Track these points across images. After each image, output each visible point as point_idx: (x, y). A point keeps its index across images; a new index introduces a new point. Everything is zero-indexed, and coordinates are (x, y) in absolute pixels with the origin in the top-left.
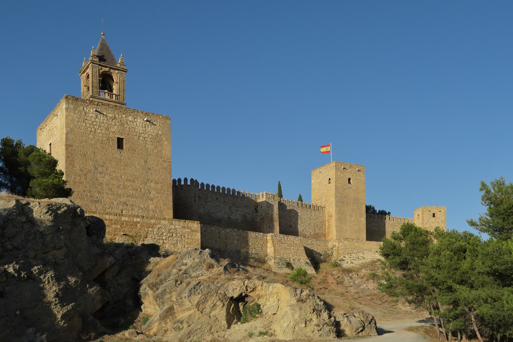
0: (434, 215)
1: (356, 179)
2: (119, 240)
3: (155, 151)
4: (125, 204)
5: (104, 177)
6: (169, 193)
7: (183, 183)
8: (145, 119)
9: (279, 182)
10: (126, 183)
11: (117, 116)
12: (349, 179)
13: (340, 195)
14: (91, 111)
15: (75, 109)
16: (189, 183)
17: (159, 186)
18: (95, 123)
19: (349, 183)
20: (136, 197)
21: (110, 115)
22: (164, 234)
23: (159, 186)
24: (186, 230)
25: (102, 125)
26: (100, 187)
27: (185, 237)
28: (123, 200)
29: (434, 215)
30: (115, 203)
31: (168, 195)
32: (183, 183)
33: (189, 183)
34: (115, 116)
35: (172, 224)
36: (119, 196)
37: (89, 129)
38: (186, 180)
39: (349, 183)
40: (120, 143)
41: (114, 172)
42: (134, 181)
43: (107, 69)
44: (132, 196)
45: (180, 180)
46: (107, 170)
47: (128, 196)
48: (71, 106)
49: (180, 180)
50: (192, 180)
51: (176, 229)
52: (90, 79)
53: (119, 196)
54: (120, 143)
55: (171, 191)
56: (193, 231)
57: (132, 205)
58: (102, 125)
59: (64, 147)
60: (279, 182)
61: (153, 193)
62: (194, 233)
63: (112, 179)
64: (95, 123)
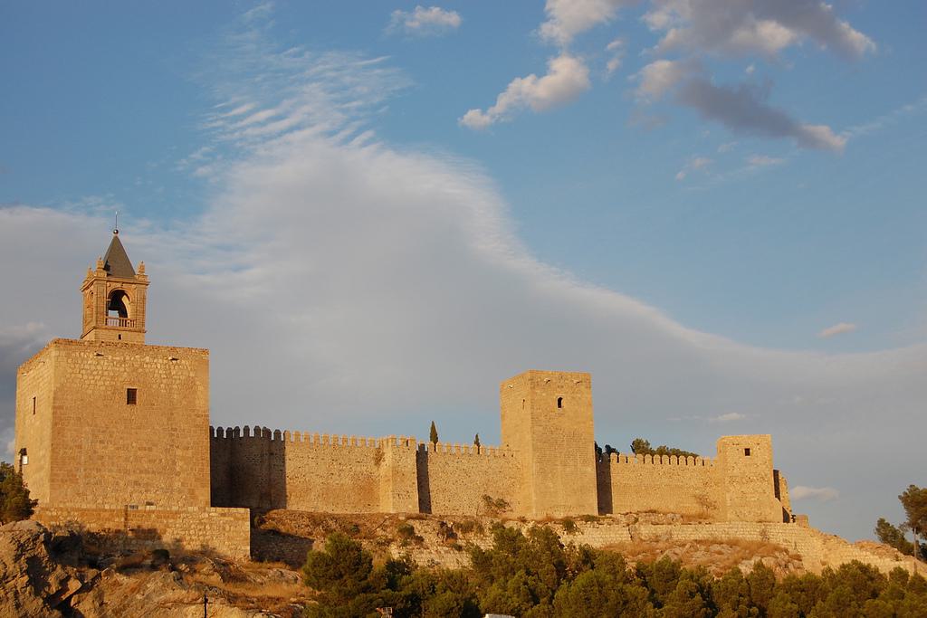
0: (747, 452)
1: (573, 398)
2: (242, 510)
3: (184, 402)
4: (136, 483)
5: (105, 448)
6: (204, 462)
7: (242, 435)
8: (170, 358)
9: (433, 428)
10: (139, 453)
11: (128, 358)
12: (560, 400)
13: (541, 428)
14: (91, 356)
15: (68, 356)
16: (252, 434)
17: (190, 453)
18: (95, 373)
19: (560, 405)
20: (153, 472)
21: (118, 358)
22: (192, 526)
23: (190, 453)
24: (226, 519)
25: (106, 373)
26: (100, 462)
27: (224, 529)
28: (133, 478)
29: (747, 452)
30: (122, 484)
31: (203, 465)
32: (242, 435)
33: (252, 434)
34: (125, 358)
35: (205, 511)
36: (127, 472)
37: (87, 382)
38: (247, 429)
39: (560, 405)
40: (131, 396)
41: (121, 438)
42: (150, 450)
43: (119, 285)
44: (147, 472)
45: (237, 430)
46: (111, 436)
47: (141, 472)
48: (63, 353)
49: (237, 430)
50: (257, 430)
51: (210, 518)
52: (94, 297)
53: (127, 472)
54: (131, 396)
55: (209, 459)
56: (237, 519)
57: (147, 484)
58: (106, 373)
59: (50, 410)
60: (433, 428)
61: (181, 463)
62: (240, 522)
63: (118, 449)
64: (95, 373)
